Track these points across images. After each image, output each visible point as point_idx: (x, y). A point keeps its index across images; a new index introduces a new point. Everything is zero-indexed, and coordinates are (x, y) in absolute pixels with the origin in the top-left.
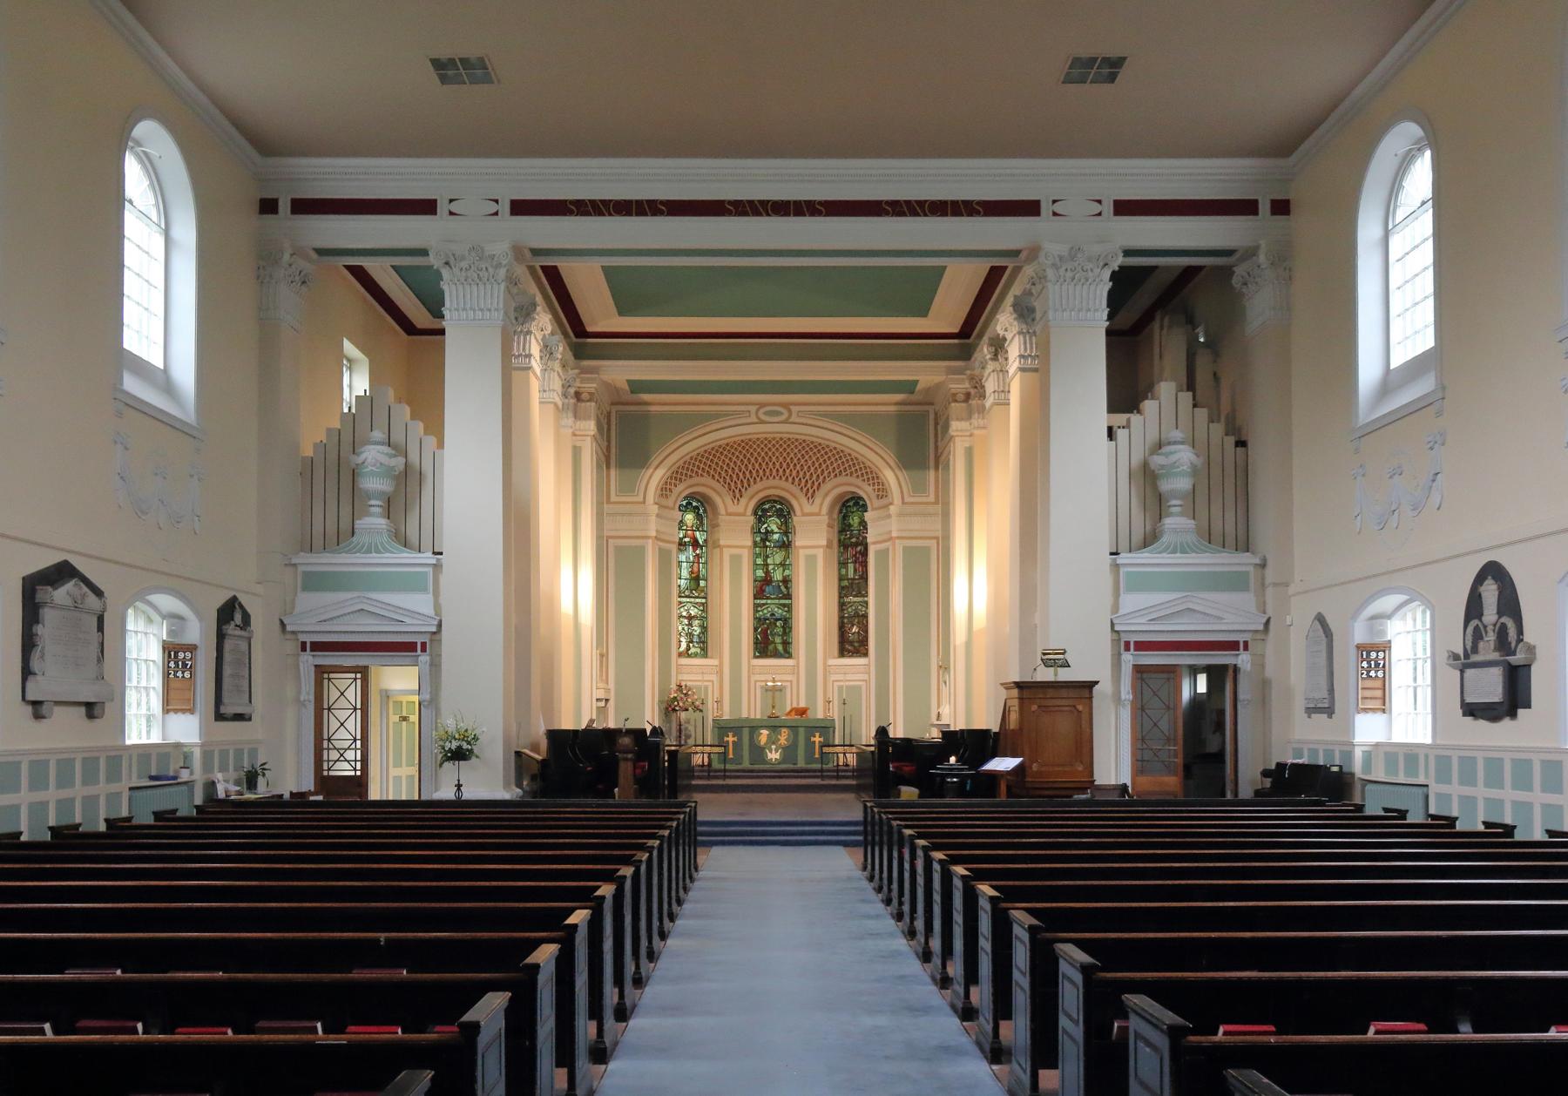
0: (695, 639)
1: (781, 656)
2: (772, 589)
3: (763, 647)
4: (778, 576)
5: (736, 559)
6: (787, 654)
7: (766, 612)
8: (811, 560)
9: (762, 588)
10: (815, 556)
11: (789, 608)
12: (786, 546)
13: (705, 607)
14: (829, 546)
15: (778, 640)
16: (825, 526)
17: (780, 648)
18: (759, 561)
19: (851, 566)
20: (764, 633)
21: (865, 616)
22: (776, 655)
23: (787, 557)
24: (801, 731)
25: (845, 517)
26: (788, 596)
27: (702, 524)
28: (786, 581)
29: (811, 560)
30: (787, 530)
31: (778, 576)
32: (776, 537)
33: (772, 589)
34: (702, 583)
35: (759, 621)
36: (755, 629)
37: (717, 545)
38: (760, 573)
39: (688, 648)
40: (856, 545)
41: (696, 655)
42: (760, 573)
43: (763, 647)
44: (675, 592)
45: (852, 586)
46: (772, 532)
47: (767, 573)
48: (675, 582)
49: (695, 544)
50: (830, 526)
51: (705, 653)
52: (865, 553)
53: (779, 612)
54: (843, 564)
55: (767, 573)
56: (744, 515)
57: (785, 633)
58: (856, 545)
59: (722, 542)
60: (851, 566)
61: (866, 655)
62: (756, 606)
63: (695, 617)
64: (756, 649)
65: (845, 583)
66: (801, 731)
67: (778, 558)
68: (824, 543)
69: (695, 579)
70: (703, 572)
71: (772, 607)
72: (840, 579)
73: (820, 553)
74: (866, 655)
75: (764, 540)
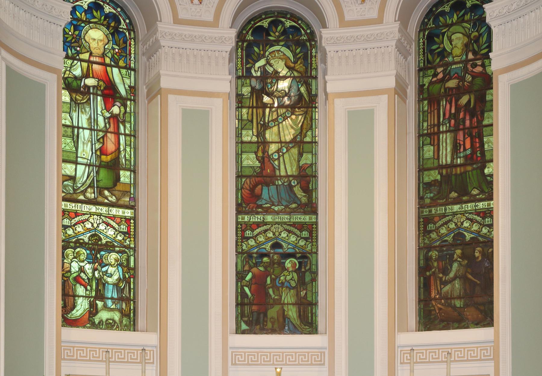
0: (110, 292)
1: (295, 330)
2: (276, 196)
3: (256, 311)
4: (287, 166)
5: (196, 121)
6: (308, 324)
7: (261, 241)
8: (360, 122)
9: (253, 189)
10: (369, 114)
11: (311, 231)
12: (305, 103)
13: (131, 228)
14: (400, 90)
15: (288, 297)
16: (392, 49)
17: (292, 313)
18: (248, 136)
19: (446, 142)
20: (259, 284)
21: (489, 243)
22: (281, 326)
23: (309, 125)
24: (128, 213)
25: (430, 39)
26: (311, 208)
27: (124, 52)
28: (307, 178)
29: (360, 122)
30: (306, 73)
31: (287, 166)
32: (284, 85)
33: (276, 196)
34: (125, 176)
35: (247, 259)
36: (240, 276)
37: (155, 91)
38: (250, 160)
39: (93, 310)
40: (459, 92)
41: (110, 325)
42: (250, 160)
43: (256, 311)
44: (52, 191)
45: (453, 181)
46: (276, 76)
47: (265, 159)
48: (53, 171)
49: (110, 93)
50: (401, 49)
51: (129, 320)
52: (482, 105)
53: (290, 240)
54: (428, 136)
55: (265, 159)
56: (215, 24)
57: (302, 283)
58: (459, 92)
59: (165, 83)
60: (446, 142)
61: (485, 317)
62: (242, 230)
63: (109, 247)
64: (240, 316)
65: (435, 175)
66: (128, 213)
67: (288, 130)
68: (391, 83)
69: (110, 165)
70: (126, 153)
71: (276, 225)
72: (421, 169)
73: (381, 107)
74: (485, 317)
75: (257, 93)
